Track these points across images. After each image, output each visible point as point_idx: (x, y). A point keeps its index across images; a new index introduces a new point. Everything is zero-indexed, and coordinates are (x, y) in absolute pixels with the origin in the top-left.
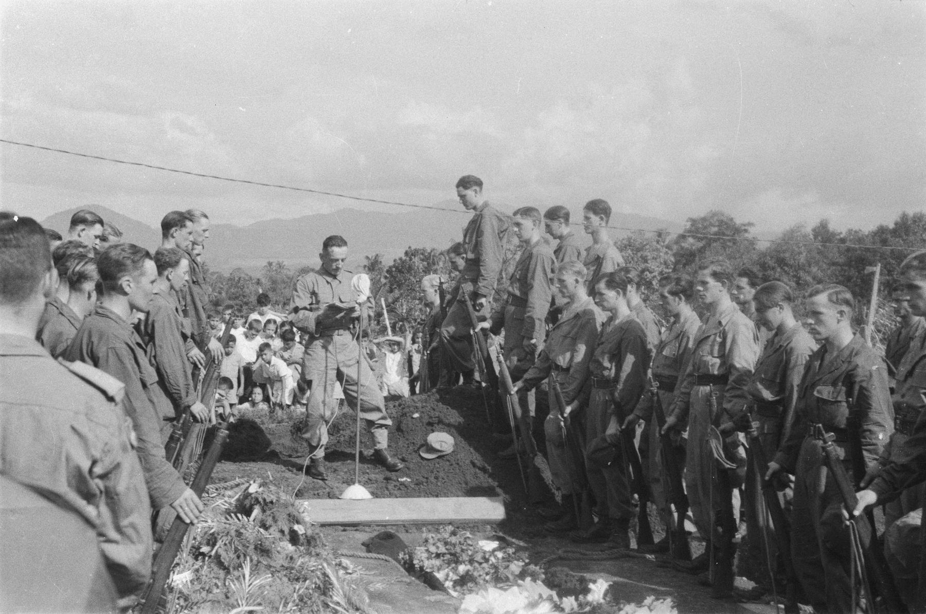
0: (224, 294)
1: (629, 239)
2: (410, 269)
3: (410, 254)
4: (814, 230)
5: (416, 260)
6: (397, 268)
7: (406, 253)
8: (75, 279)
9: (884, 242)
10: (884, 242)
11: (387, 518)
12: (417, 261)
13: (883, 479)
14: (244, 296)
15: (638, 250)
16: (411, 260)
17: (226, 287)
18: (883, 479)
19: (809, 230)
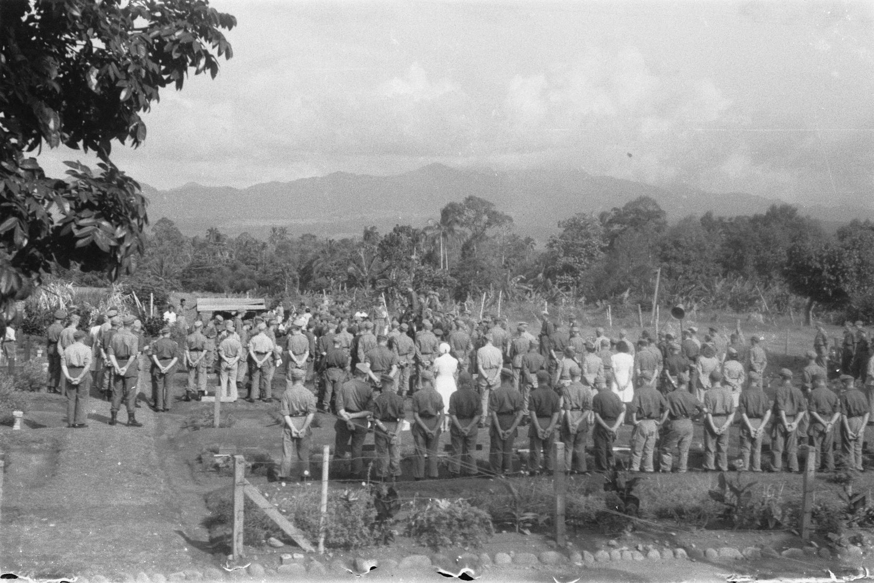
0: (234, 257)
1: (574, 219)
2: (398, 243)
3: (399, 230)
4: (701, 220)
5: (403, 236)
6: (387, 242)
7: (395, 230)
8: (425, 537)
9: (755, 228)
10: (755, 228)
11: (184, 184)
12: (405, 239)
13: (465, 450)
14: (251, 259)
15: (582, 228)
16: (398, 235)
17: (235, 251)
18: (465, 450)
19: (698, 220)
